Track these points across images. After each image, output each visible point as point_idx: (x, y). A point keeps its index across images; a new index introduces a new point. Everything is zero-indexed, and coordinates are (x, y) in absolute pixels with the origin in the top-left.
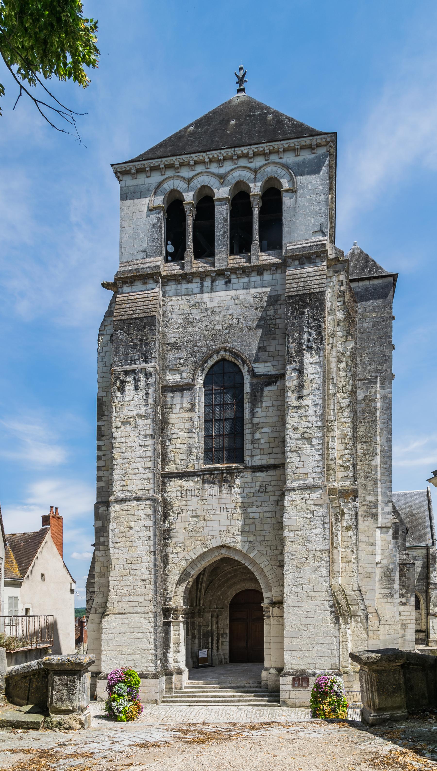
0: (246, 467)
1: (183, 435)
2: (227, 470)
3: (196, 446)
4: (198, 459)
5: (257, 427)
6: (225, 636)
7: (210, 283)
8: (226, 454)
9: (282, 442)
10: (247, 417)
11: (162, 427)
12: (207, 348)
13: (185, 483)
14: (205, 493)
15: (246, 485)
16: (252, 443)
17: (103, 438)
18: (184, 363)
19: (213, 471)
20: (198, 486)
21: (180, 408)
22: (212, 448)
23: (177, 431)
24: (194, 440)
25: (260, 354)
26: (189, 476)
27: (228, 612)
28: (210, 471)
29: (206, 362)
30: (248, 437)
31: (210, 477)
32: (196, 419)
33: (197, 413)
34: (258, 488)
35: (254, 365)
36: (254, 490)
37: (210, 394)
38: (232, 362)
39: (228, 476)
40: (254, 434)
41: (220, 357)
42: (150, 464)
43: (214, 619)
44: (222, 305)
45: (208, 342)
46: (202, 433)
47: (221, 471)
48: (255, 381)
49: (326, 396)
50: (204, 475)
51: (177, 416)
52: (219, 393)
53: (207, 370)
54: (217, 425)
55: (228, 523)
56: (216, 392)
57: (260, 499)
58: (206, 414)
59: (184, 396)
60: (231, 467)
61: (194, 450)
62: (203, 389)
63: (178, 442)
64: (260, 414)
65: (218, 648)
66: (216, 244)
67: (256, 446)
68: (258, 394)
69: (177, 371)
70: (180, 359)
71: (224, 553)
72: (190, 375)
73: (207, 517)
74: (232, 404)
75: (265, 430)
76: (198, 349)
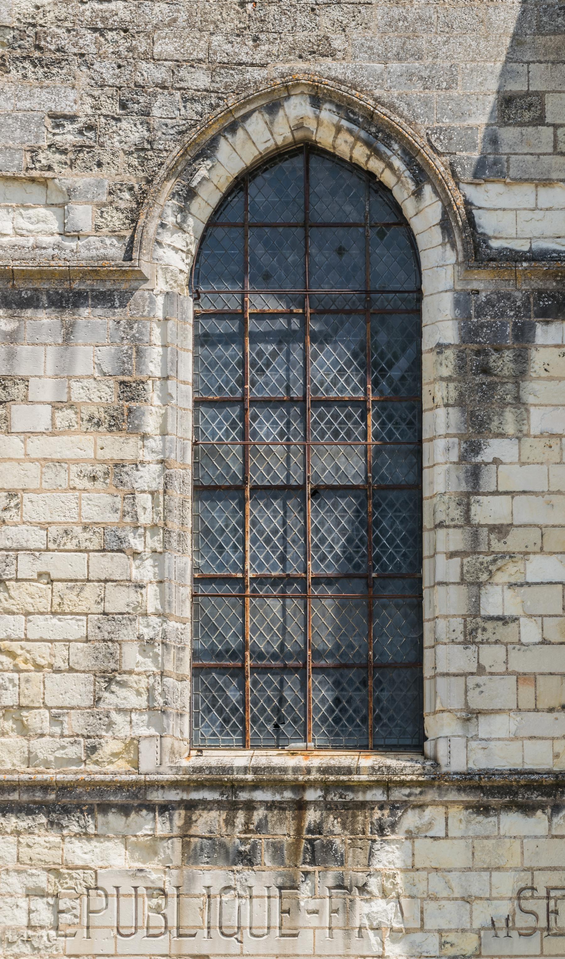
0: (436, 779)
2: (327, 787)
3: (148, 633)
4: (157, 711)
5: (497, 546)
8: (320, 693)
10: (440, 487)
12: (213, 72)
13: (79, 852)
14: (194, 918)
15: (437, 884)
16: (470, 638)
18: (80, 149)
19: (242, 786)
20: (156, 875)
21: (56, 406)
22: (237, 654)
23: (36, 539)
24: (133, 596)
25: (508, 134)
26: (104, 808)
28: (229, 791)
29: (206, 150)
30: (443, 604)
31: (230, 822)
32: (148, 477)
33: (155, 443)
34: (504, 908)
35: (477, 195)
36: (482, 915)
37: (227, 339)
38: (354, 167)
39: (333, 824)
40: (480, 585)
41: (283, 133)
45: (217, 39)
46: (183, 562)
47: (293, 797)
48: (483, 282)
50: (191, 806)
51: (40, 447)
52: (283, 338)
53: (215, 199)
54: (264, 517)
56: (262, 327)
58: (203, 454)
59: (80, 335)
60: (349, 771)
61: (132, 656)
62: (189, 306)
63: (44, 604)
64: (510, 477)
67: (491, 656)
68: (504, 363)
69: (36, 190)
70: (59, 119)
72: (116, 219)
74: (354, 403)
75: (540, 568)
76: (160, 74)
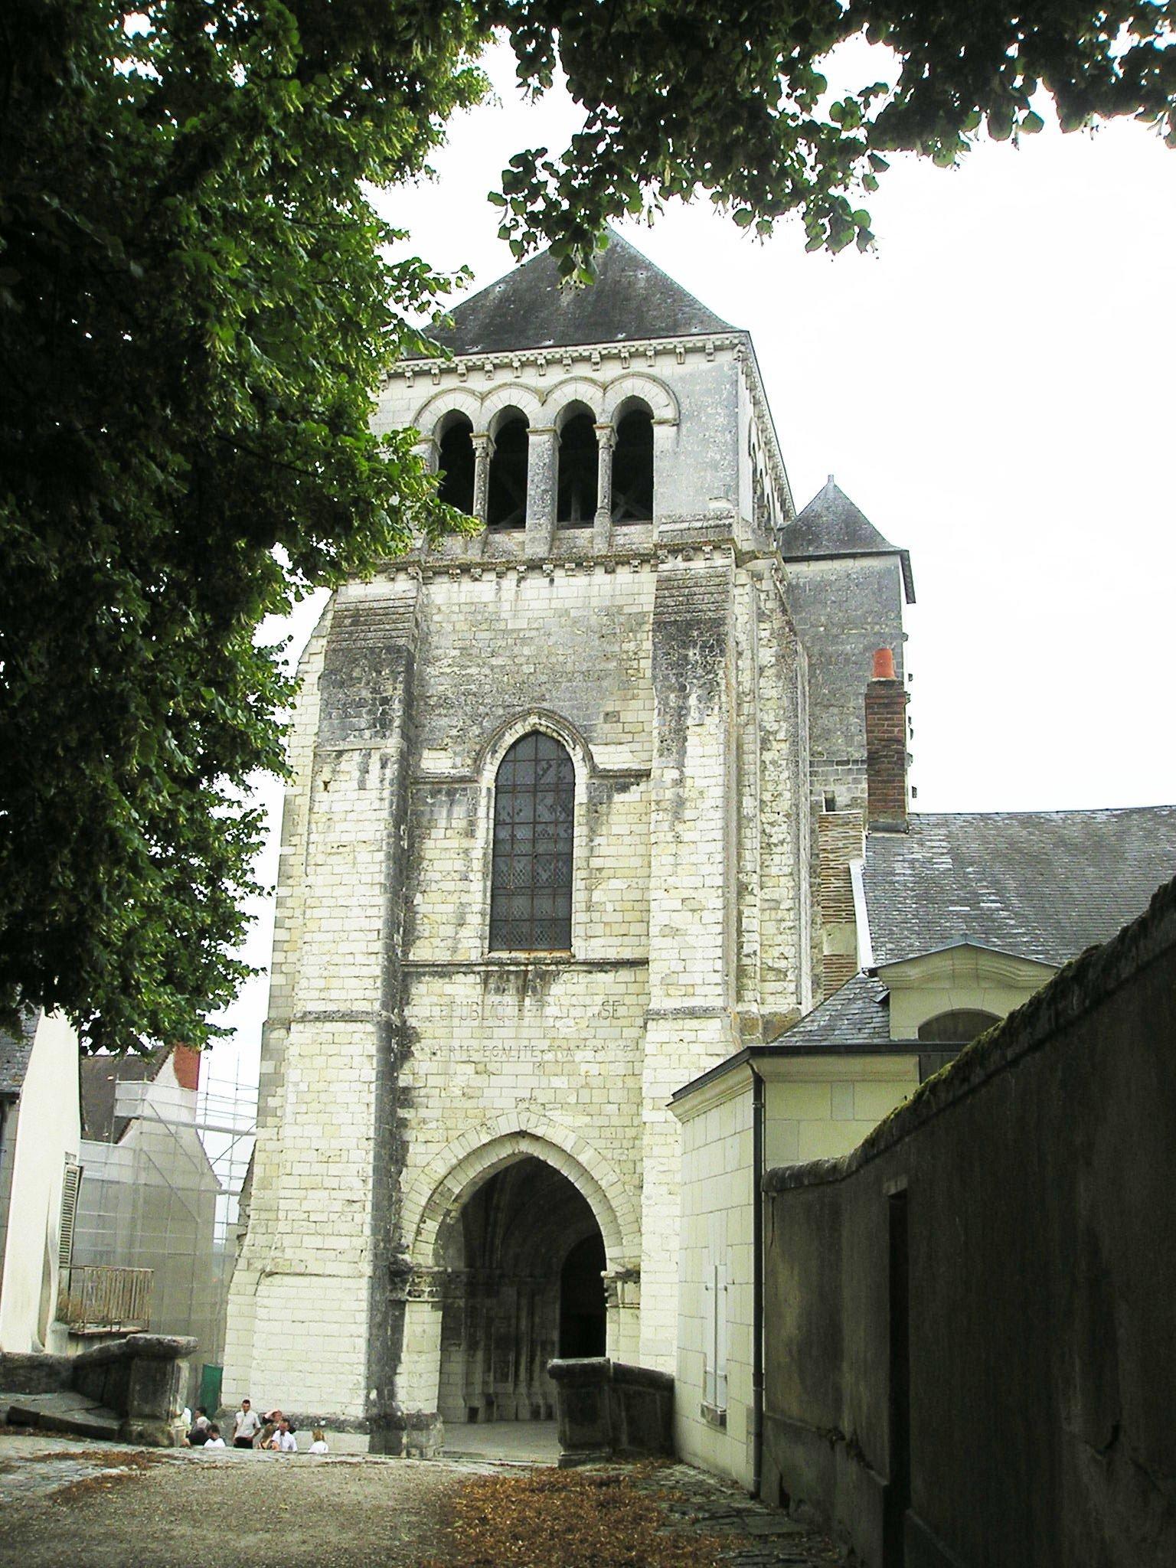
1: (450, 886)
6: (549, 1348)
7: (515, 582)
9: (643, 910)
11: (405, 868)
13: (449, 989)
16: (588, 909)
17: (290, 882)
23: (438, 876)
27: (557, 1287)
30: (579, 897)
34: (596, 1010)
41: (528, 729)
42: (378, 946)
43: (524, 1302)
44: (535, 626)
49: (737, 823)
55: (533, 1082)
57: (601, 1033)
64: (603, 851)
65: (531, 1379)
66: (528, 512)
67: (596, 916)
68: (603, 809)
71: (525, 1147)
73: (491, 1067)
75: (615, 884)
76: (487, 710)
